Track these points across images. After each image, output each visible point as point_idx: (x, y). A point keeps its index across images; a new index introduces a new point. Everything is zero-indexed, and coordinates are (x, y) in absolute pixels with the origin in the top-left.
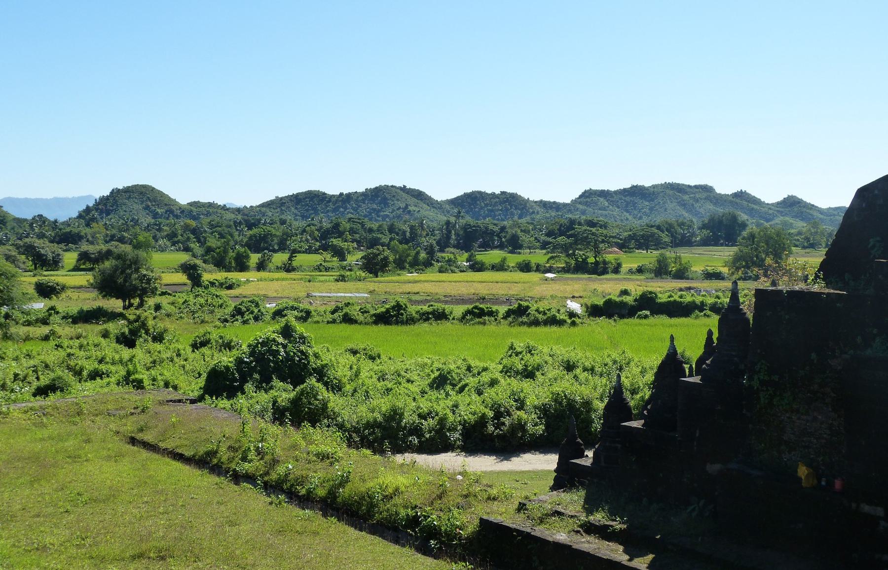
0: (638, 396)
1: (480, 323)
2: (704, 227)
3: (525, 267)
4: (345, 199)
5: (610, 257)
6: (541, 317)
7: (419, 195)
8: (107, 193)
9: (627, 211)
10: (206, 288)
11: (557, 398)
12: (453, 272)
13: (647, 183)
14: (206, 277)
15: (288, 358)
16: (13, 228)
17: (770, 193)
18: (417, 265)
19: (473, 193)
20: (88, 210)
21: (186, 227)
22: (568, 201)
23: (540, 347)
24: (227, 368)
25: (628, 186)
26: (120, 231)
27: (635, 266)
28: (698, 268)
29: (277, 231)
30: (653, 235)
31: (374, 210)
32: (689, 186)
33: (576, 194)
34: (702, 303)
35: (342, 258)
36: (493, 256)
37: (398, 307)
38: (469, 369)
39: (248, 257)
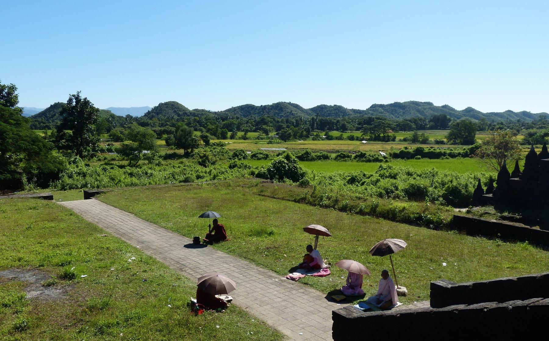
0: (446, 186)
1: (344, 161)
2: (431, 121)
3: (351, 138)
4: (264, 108)
5: (391, 133)
6: (371, 158)
7: (297, 106)
8: (157, 105)
9: (392, 114)
10: (212, 146)
11: (412, 186)
12: (319, 140)
13: (402, 101)
14: (212, 141)
15: (289, 169)
16: (117, 120)
17: (459, 106)
18: (302, 137)
19: (321, 105)
20: (149, 113)
21: (195, 120)
22: (365, 109)
23: (394, 167)
24: (264, 173)
25: (393, 102)
26: (166, 122)
27: (402, 138)
28: (432, 139)
29: (236, 122)
30: (408, 124)
31: (277, 113)
32: (421, 103)
33: (368, 106)
34: (444, 152)
35: (267, 134)
36: (335, 133)
37: (307, 153)
38: (364, 175)
39: (227, 133)
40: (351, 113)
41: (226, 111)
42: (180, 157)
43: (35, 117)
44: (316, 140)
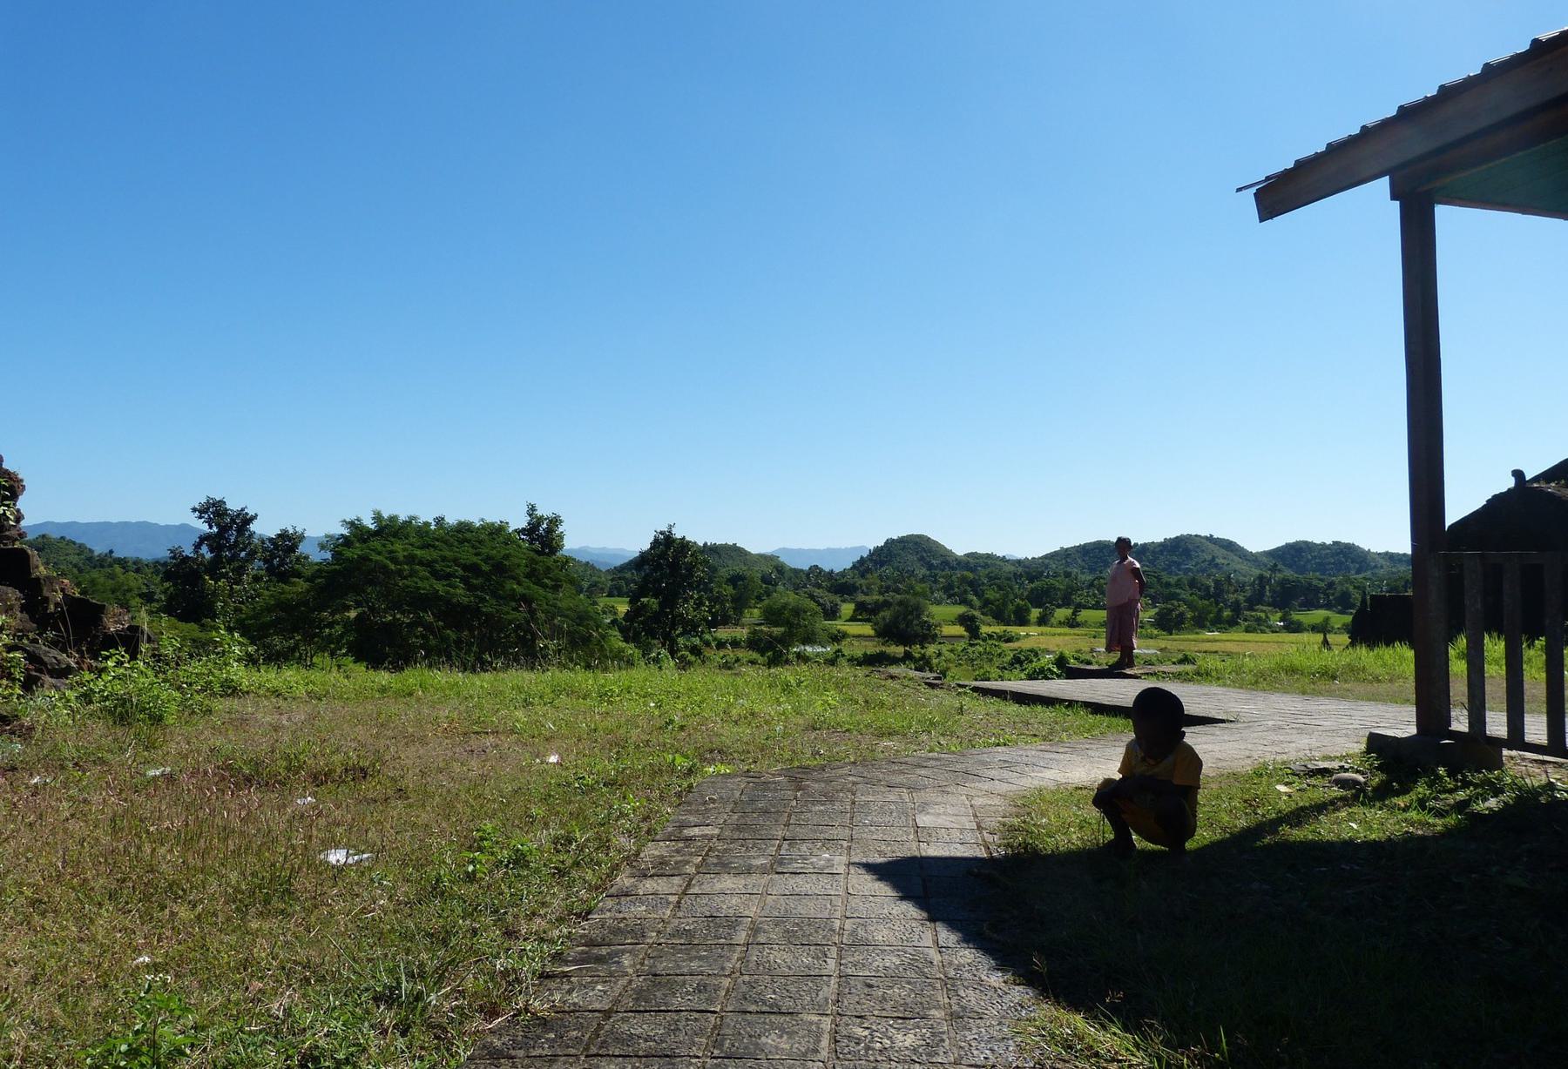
7: (1229, 546)
12: (1263, 632)
14: (984, 629)
19: (1297, 543)
39: (1028, 611)
40: (1382, 561)
41: (1046, 557)
42: (894, 661)
43: (622, 568)
44: (1254, 631)
